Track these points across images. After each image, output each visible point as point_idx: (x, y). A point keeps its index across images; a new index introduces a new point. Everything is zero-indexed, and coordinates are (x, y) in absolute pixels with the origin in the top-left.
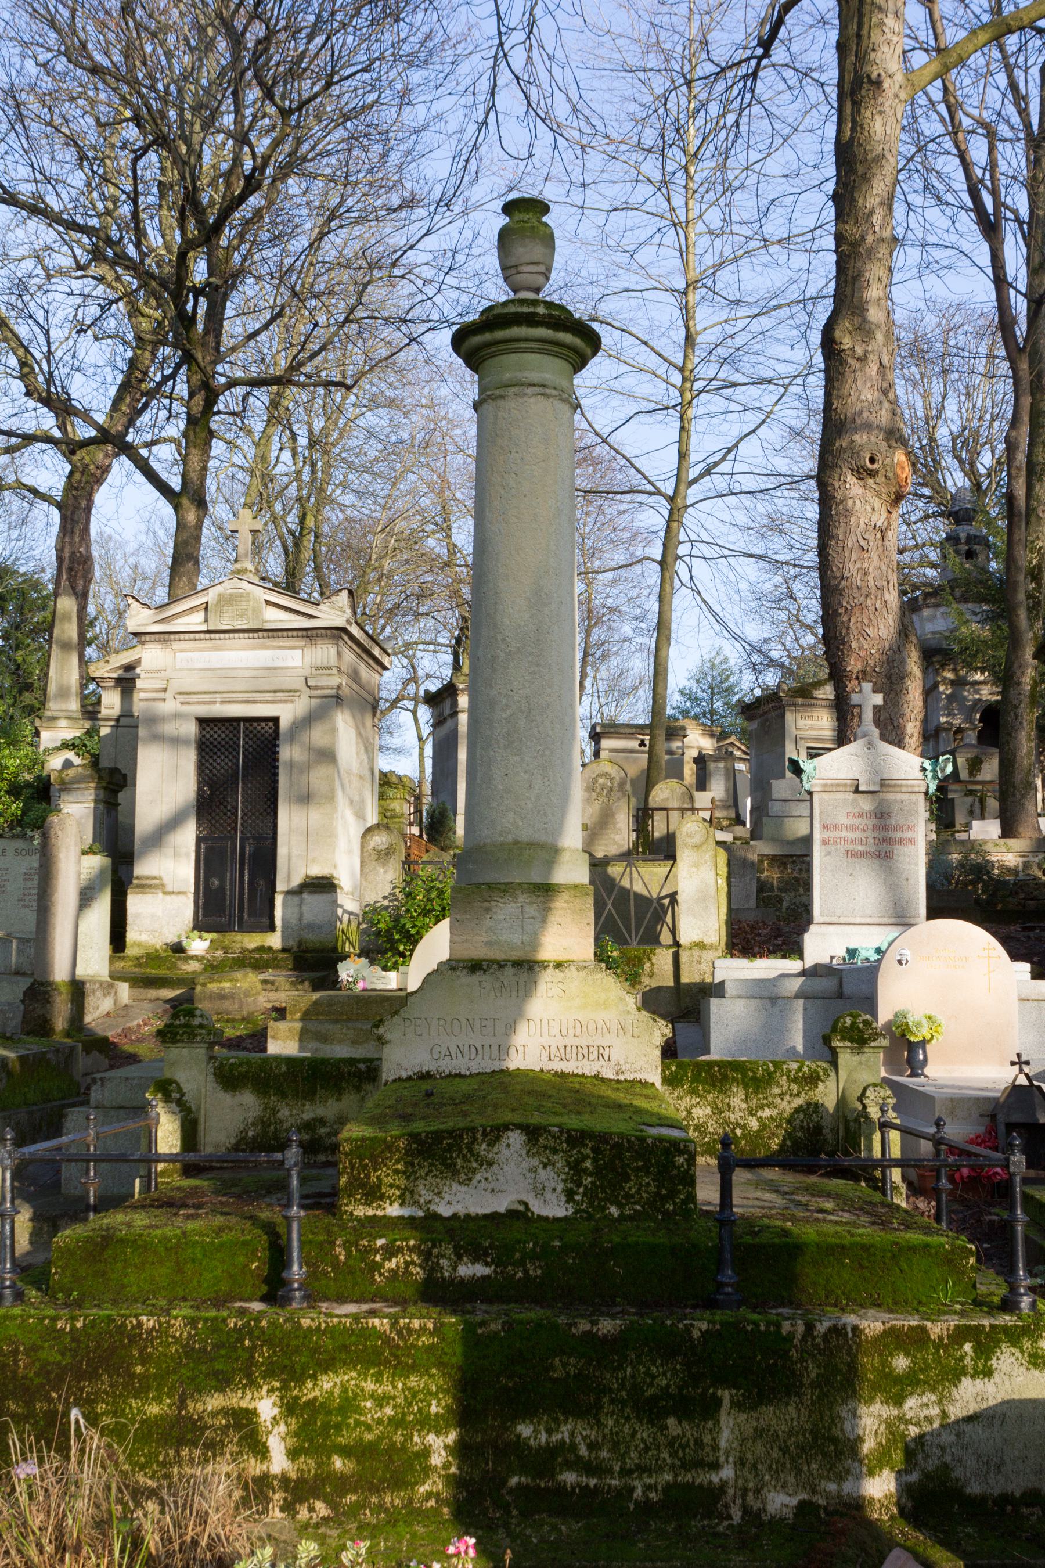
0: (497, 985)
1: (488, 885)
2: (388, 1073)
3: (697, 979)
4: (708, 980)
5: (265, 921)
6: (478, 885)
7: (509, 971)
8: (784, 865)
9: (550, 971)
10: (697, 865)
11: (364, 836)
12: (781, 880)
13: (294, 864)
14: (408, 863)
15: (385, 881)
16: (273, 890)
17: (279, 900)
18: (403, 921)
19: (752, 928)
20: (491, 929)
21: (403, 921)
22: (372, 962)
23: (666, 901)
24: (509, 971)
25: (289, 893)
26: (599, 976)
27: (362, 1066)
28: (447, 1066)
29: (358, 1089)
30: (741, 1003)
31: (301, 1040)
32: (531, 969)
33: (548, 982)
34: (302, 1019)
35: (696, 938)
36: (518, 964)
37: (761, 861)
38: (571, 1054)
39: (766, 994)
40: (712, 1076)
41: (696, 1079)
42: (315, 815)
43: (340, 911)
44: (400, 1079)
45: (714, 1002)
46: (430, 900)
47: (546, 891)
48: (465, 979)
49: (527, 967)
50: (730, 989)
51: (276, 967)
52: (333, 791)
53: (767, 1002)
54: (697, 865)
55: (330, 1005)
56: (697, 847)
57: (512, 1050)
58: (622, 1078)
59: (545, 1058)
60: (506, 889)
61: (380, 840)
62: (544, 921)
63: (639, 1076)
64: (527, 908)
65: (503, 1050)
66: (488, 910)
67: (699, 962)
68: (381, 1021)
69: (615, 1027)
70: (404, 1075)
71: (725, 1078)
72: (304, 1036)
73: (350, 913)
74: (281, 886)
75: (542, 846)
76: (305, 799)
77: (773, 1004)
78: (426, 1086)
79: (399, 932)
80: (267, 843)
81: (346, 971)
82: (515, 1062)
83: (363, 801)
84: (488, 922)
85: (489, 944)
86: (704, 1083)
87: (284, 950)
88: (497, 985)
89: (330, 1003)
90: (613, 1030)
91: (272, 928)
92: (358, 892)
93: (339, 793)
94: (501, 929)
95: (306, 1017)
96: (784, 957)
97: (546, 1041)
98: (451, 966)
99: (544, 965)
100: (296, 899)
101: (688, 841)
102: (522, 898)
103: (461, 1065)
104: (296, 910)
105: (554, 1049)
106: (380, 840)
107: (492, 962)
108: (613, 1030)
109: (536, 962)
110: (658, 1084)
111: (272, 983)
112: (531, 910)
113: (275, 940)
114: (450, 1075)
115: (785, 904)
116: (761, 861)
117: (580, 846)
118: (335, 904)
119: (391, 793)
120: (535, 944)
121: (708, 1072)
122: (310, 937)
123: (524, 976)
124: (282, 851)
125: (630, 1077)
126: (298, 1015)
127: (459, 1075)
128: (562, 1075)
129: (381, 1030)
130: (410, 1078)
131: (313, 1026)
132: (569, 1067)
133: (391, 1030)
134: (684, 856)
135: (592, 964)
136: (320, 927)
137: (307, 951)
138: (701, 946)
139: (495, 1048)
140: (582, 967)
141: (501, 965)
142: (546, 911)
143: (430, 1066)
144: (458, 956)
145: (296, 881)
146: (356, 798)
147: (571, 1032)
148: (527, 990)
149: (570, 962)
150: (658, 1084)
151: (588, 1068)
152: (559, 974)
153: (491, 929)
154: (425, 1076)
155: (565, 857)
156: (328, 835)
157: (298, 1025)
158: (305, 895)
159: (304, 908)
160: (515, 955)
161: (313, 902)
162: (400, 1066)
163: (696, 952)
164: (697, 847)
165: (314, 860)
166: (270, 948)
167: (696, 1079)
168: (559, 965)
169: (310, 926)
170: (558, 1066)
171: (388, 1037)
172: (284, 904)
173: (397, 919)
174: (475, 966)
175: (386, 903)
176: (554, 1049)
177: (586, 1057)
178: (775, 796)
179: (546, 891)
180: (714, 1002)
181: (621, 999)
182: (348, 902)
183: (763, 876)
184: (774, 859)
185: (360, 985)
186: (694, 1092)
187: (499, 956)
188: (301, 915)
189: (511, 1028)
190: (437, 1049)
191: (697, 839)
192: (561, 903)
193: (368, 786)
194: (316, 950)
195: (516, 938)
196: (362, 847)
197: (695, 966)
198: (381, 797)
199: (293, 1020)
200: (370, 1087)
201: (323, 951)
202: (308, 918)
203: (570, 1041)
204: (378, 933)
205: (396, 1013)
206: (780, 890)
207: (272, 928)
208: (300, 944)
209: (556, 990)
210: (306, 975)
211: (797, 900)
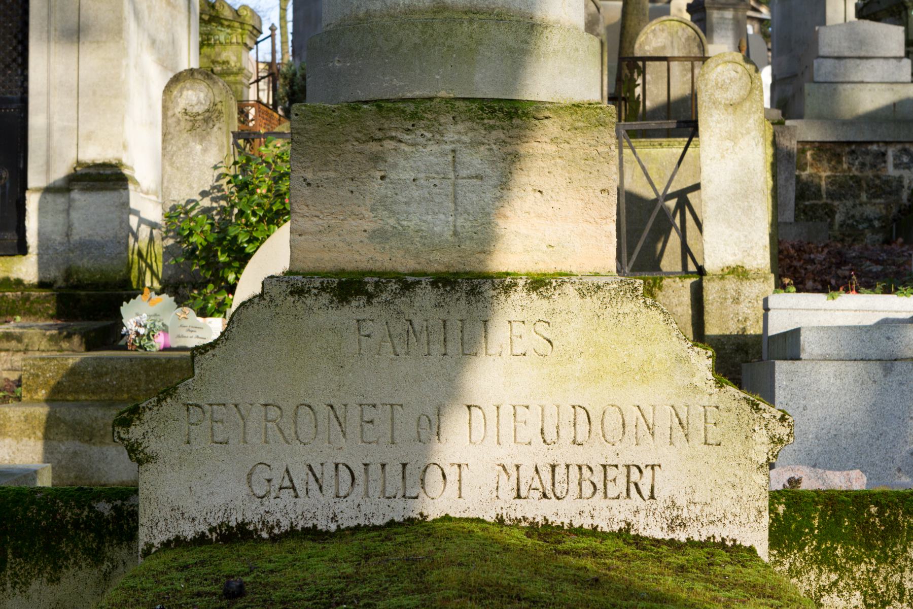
0: (400, 327)
1: (378, 104)
2: (152, 531)
3: (732, 329)
4: (754, 329)
5: (11, 237)
6: (355, 106)
7: (426, 296)
8: (838, 157)
9: (519, 296)
10: (733, 137)
11: (168, 89)
12: (832, 181)
13: (57, 141)
14: (245, 136)
15: (204, 167)
16: (24, 188)
17: (32, 202)
18: (232, 231)
19: (799, 250)
20: (383, 203)
21: (232, 231)
22: (181, 301)
23: (672, 204)
24: (426, 296)
25: (49, 190)
26: (629, 306)
27: (104, 508)
28: (286, 512)
29: (96, 556)
30: (828, 370)
31: (46, 438)
32: (474, 292)
33: (514, 322)
34: (49, 401)
35: (731, 260)
36: (445, 281)
37: (802, 152)
38: (567, 483)
39: (873, 353)
40: (865, 526)
41: (830, 532)
42: (92, 60)
43: (133, 221)
44: (178, 542)
45: (782, 368)
46: (279, 195)
47: (509, 116)
48: (323, 315)
49: (468, 287)
50: (809, 344)
51: (28, 313)
52: (120, 20)
53: (875, 368)
54: (733, 137)
55: (98, 375)
56: (733, 106)
57: (434, 475)
58: (681, 536)
59: (507, 493)
60: (415, 113)
61: (194, 97)
62: (504, 184)
63: (719, 532)
64: (465, 156)
65: (414, 474)
66: (376, 159)
67: (736, 301)
68: (136, 411)
69: (664, 421)
70: (189, 532)
71: (893, 529)
72: (52, 429)
73: (153, 226)
74: (36, 179)
75: (500, 17)
76: (75, 33)
77: (887, 371)
78: (231, 563)
79: (228, 250)
80: (12, 110)
81: (135, 316)
82: (439, 503)
83: (174, 42)
84: (376, 187)
85: (380, 236)
86: (847, 539)
87: (42, 285)
88: (400, 327)
89: (99, 371)
90: (662, 428)
91: (22, 249)
92: (163, 188)
93: (131, 25)
94: (401, 205)
95: (56, 396)
96: (887, 291)
97: (508, 454)
98: (294, 285)
99: (504, 283)
100: (60, 201)
101: (719, 95)
102: (455, 132)
103: (318, 509)
104: (61, 218)
105: (527, 473)
106: (194, 97)
107: (384, 277)
108: (662, 428)
109: (488, 277)
110: (763, 550)
111: (19, 339)
112: (474, 160)
113: (27, 269)
114: (292, 533)
115: (838, 218)
116: (802, 152)
117: (580, 20)
118: (125, 208)
119: (222, 35)
120: (486, 239)
121: (856, 516)
122: (85, 263)
123: (458, 308)
124: (36, 121)
125: (698, 533)
126: (42, 394)
127: (313, 534)
128: (545, 532)
129: (135, 432)
130: (201, 540)
131: (66, 412)
132: (562, 512)
133: (160, 430)
134: (712, 123)
135: (614, 282)
136: (100, 246)
137: (79, 286)
138: (739, 273)
139: (394, 470)
140: (591, 288)
141: (406, 284)
142: (509, 162)
143: (246, 511)
144: (308, 264)
145: (60, 172)
146: (162, 36)
147: (567, 433)
148: (467, 340)
149: (563, 277)
150: (763, 550)
151: (606, 514)
152: (538, 304)
153: (383, 203)
154: (236, 535)
155: (552, 42)
156: (111, 93)
157: (42, 411)
158: (76, 195)
159: (74, 215)
160: (439, 262)
161: (89, 206)
162: (179, 513)
163: (731, 284)
164: (733, 106)
165: (89, 137)
166: (19, 282)
167: (830, 532)
168: (538, 284)
169: (85, 246)
170: (536, 510)
171: (152, 446)
172: (41, 209)
173: (221, 229)
174: (349, 287)
175: (206, 203)
176: (527, 473)
177: (600, 489)
178: (824, 50)
179: (509, 116)
180: (782, 368)
181: (680, 360)
182: (147, 205)
183: (804, 174)
184: (821, 147)
185: (159, 341)
186: (825, 560)
187: (404, 263)
188: (70, 226)
189: (431, 425)
190: (262, 474)
191: (734, 93)
192: (543, 147)
193: (182, 17)
194: (95, 285)
195: (441, 224)
196: (165, 108)
197: (731, 308)
198: (205, 42)
199: (33, 402)
200: (121, 553)
201: (106, 285)
202: (81, 231)
203: (565, 454)
204: (191, 254)
205: (168, 392)
206: (830, 195)
207: (22, 249)
208: (68, 274)
209: (531, 340)
210: (75, 325)
211: (857, 212)
